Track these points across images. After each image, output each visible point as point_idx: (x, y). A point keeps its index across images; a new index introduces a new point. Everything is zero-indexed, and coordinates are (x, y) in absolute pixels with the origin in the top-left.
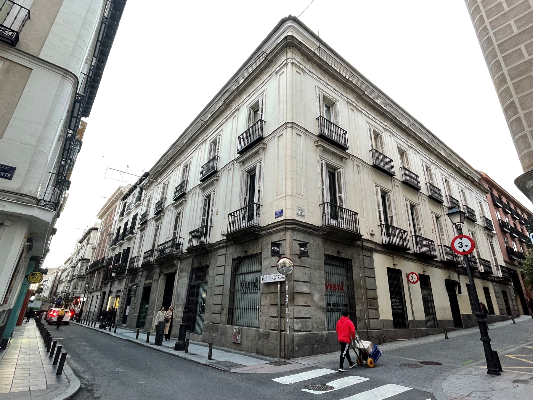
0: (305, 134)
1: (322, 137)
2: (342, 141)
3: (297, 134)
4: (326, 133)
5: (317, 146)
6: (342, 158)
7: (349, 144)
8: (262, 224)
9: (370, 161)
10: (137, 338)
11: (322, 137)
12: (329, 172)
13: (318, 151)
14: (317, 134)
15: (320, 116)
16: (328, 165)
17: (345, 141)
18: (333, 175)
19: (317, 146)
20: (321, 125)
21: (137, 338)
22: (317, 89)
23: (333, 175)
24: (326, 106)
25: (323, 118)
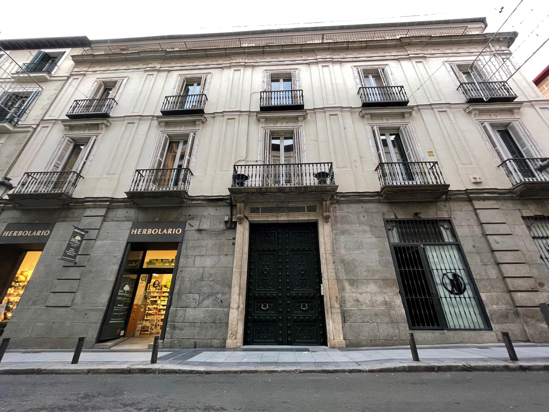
0: (341, 111)
1: (472, 101)
2: (506, 94)
3: (541, 108)
4: (474, 95)
5: (470, 113)
6: (511, 111)
7: (515, 91)
8: (74, 196)
9: (462, 99)
10: (416, 358)
11: (472, 101)
12: (498, 131)
13: (473, 117)
14: (361, 105)
15: (461, 84)
16: (493, 125)
17: (508, 92)
18: (505, 133)
19: (363, 117)
20: (465, 92)
21: (416, 358)
22: (446, 64)
23: (505, 133)
24: (464, 73)
25: (465, 84)
